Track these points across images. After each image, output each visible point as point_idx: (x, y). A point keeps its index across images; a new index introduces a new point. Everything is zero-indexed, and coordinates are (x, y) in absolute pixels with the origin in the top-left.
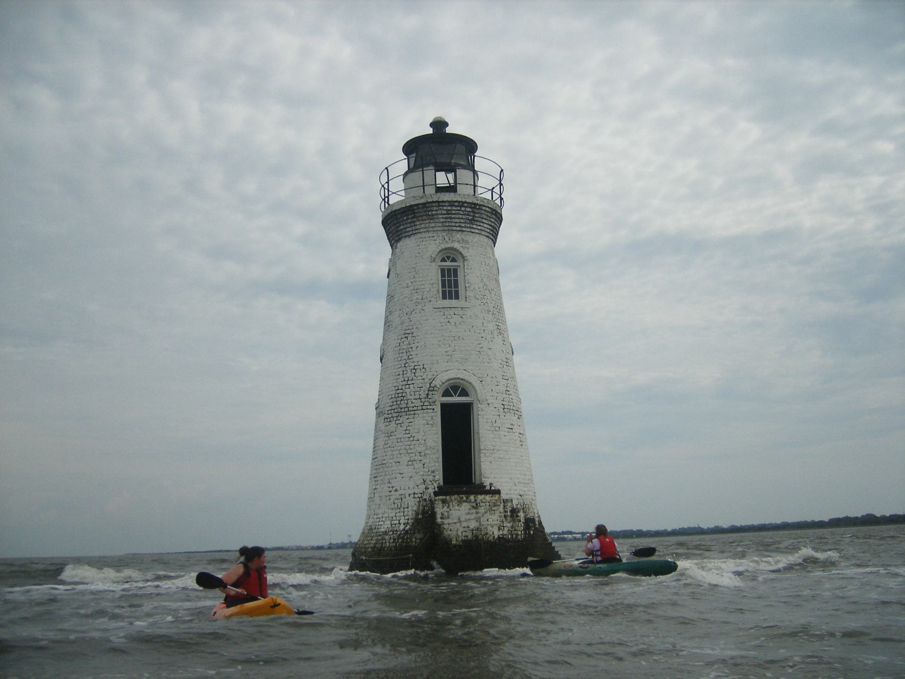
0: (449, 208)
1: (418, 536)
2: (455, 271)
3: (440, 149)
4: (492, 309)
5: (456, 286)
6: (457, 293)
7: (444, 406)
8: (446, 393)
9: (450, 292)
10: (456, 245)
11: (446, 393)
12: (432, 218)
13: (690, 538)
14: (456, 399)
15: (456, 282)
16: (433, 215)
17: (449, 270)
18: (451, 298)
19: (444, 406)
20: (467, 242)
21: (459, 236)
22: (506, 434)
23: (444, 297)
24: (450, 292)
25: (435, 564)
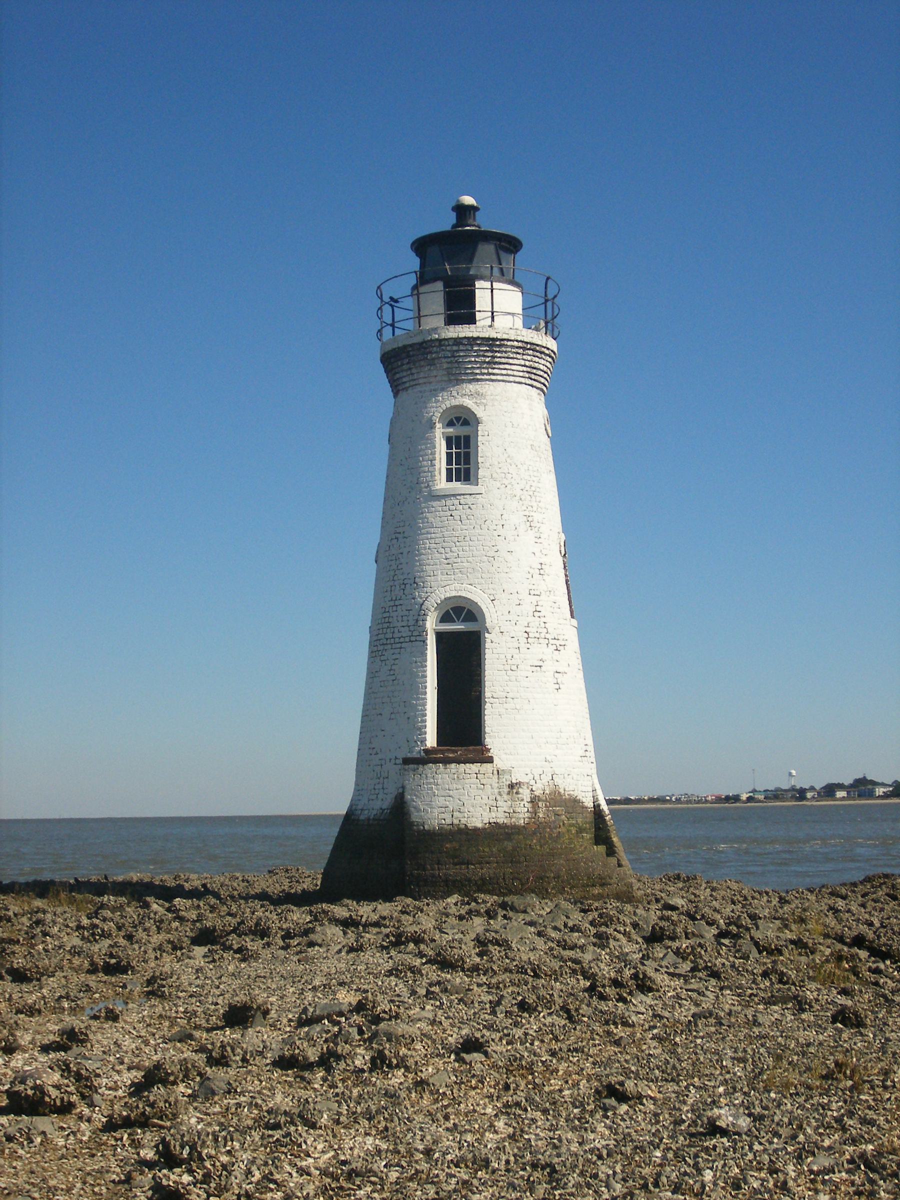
0: (455, 348)
2: (467, 439)
10: (468, 402)
12: (432, 363)
15: (449, 462)
17: (458, 438)
22: (529, 674)
23: (449, 479)
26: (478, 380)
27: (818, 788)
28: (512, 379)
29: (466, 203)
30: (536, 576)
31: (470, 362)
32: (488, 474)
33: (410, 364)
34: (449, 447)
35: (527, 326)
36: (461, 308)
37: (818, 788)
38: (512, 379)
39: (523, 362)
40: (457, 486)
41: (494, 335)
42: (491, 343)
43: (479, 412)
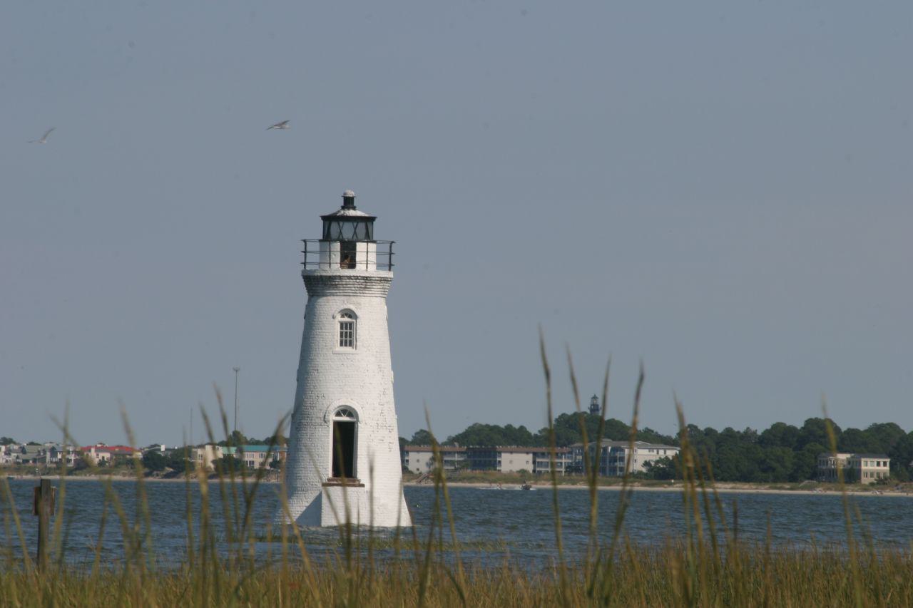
1: (140, 454)
2: (351, 324)
3: (234, 369)
4: (375, 353)
5: (341, 333)
6: (351, 342)
7: (337, 424)
8: (338, 414)
9: (346, 341)
10: (352, 307)
11: (338, 414)
13: (752, 530)
14: (345, 418)
15: (341, 336)
16: (336, 285)
17: (346, 324)
18: (346, 345)
19: (337, 424)
20: (360, 304)
21: (354, 299)
23: (341, 345)
24: (346, 341)
25: (298, 507)
26: (350, 296)
27: (441, 437)
28: (374, 295)
29: (351, 215)
30: (382, 396)
31: (342, 284)
32: (361, 344)
33: (317, 285)
34: (342, 328)
35: (342, 267)
36: (349, 259)
37: (441, 437)
38: (374, 295)
39: (379, 287)
40: (348, 349)
41: (367, 275)
42: (366, 278)
43: (358, 313)
